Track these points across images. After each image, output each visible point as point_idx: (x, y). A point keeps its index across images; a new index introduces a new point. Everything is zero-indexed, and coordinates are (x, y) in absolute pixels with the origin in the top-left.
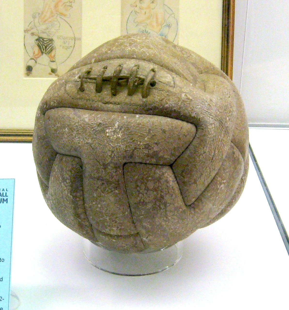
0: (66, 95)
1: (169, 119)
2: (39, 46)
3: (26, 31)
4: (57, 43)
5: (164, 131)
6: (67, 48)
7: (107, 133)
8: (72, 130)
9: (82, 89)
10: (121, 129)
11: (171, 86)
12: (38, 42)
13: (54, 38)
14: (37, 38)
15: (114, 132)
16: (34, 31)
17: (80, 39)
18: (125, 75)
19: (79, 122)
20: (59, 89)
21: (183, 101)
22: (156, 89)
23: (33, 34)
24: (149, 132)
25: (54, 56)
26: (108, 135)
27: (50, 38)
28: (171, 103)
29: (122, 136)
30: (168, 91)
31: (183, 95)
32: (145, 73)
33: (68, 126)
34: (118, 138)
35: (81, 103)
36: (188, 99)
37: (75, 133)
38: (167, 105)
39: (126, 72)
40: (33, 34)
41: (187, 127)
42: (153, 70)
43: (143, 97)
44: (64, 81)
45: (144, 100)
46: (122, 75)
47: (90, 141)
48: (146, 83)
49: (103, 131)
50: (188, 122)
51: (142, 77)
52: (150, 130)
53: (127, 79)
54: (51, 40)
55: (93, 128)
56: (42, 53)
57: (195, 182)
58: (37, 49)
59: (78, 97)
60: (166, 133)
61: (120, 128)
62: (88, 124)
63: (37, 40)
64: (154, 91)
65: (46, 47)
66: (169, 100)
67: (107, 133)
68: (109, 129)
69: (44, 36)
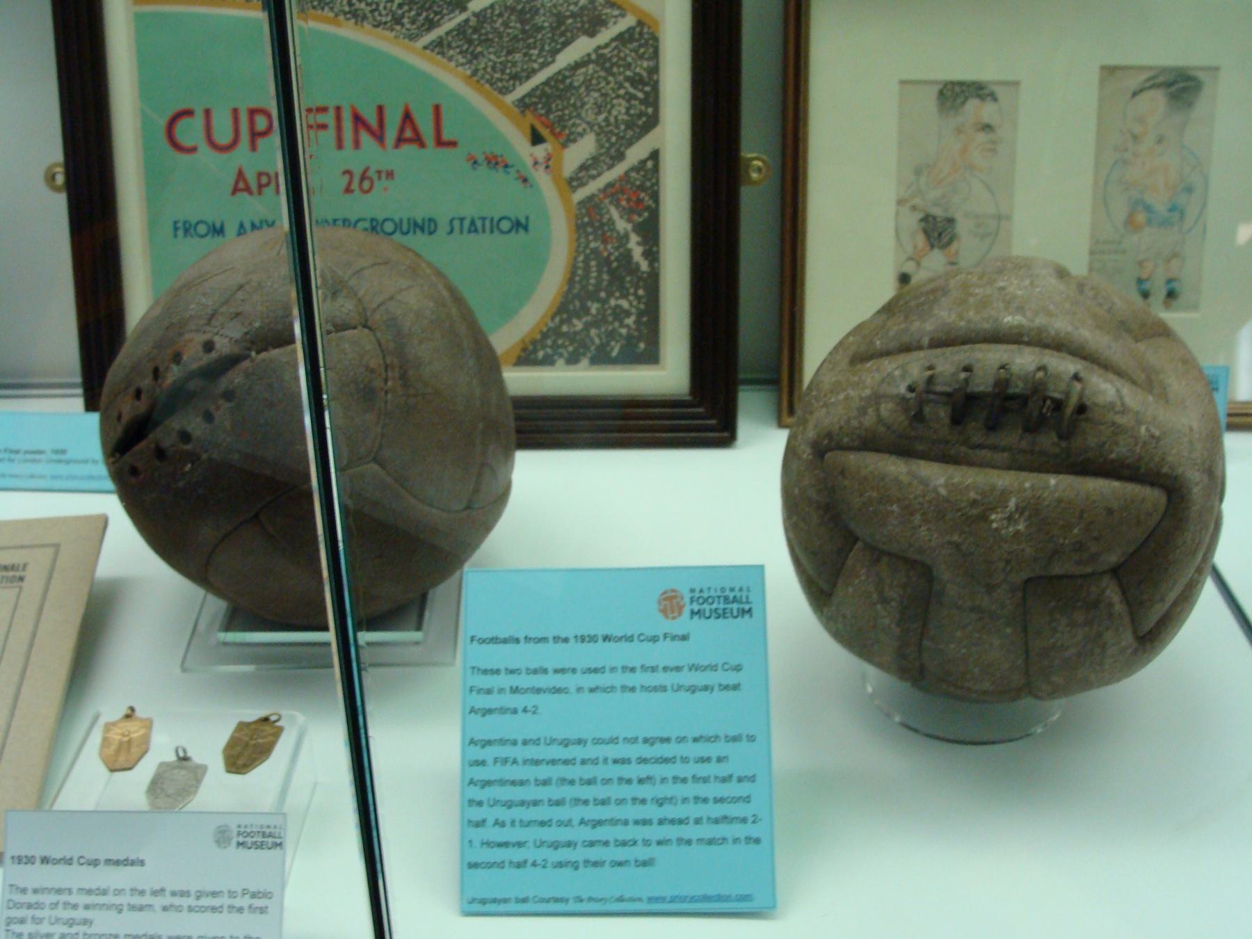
0: (882, 429)
1: (1116, 484)
2: (926, 232)
3: (900, 202)
4: (963, 227)
5: (1110, 511)
6: (983, 237)
7: (992, 521)
8: (908, 510)
9: (919, 417)
10: (1021, 514)
11: (1117, 413)
12: (923, 224)
13: (958, 216)
14: (921, 215)
15: (1010, 519)
16: (917, 201)
17: (1008, 218)
18: (1017, 390)
19: (924, 496)
20: (863, 411)
21: (1145, 443)
22: (1087, 420)
23: (914, 208)
24: (1081, 517)
25: (957, 253)
26: (994, 525)
27: (949, 215)
28: (1120, 450)
29: (1027, 528)
30: (1114, 424)
31: (1143, 429)
32: (1062, 386)
33: (899, 500)
34: (1017, 533)
35: (920, 447)
36: (1153, 436)
37: (917, 519)
38: (1113, 456)
39: (1021, 384)
40: (914, 208)
41: (1152, 496)
42: (1076, 377)
43: (1061, 437)
44: (868, 392)
45: (1064, 444)
46: (1011, 391)
47: (956, 538)
48: (1069, 411)
49: (984, 517)
50: (1152, 484)
51: (1057, 395)
52: (1082, 512)
53: (1023, 400)
54: (951, 221)
55: (959, 510)
56: (932, 246)
57: (1141, 218)
58: (921, 240)
59: (913, 433)
60: (1115, 514)
61: (1020, 510)
62: (948, 501)
63: (921, 220)
64: (1083, 425)
65: (940, 235)
66: (1116, 444)
67: (992, 521)
68: (997, 513)
69: (938, 212)
